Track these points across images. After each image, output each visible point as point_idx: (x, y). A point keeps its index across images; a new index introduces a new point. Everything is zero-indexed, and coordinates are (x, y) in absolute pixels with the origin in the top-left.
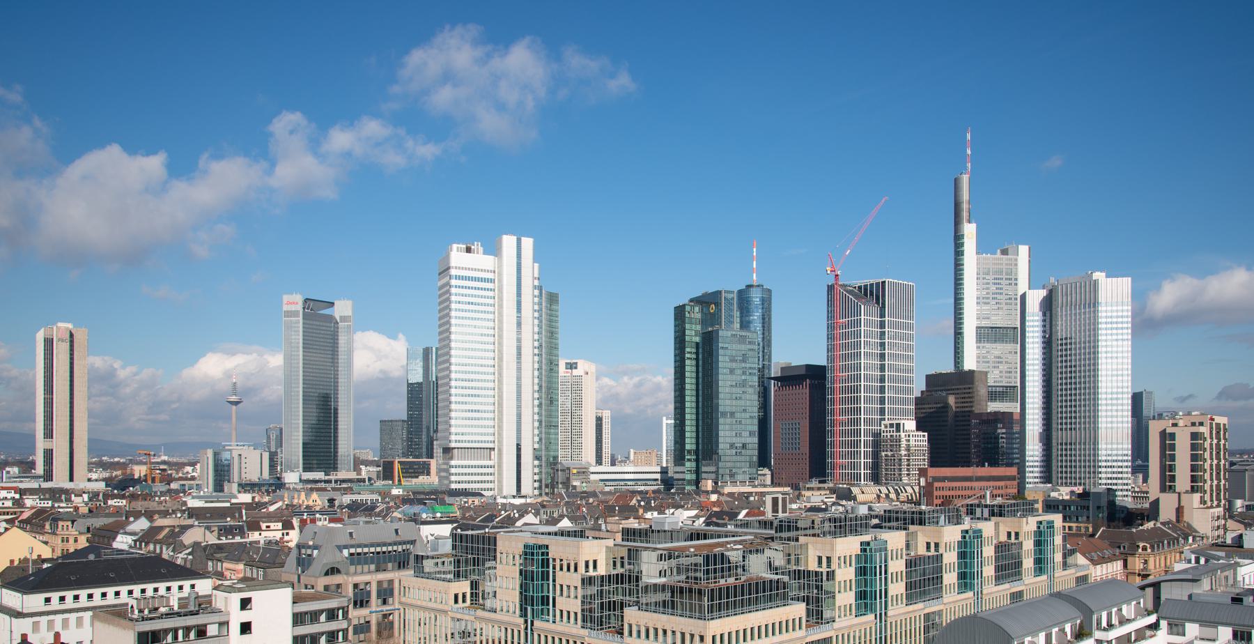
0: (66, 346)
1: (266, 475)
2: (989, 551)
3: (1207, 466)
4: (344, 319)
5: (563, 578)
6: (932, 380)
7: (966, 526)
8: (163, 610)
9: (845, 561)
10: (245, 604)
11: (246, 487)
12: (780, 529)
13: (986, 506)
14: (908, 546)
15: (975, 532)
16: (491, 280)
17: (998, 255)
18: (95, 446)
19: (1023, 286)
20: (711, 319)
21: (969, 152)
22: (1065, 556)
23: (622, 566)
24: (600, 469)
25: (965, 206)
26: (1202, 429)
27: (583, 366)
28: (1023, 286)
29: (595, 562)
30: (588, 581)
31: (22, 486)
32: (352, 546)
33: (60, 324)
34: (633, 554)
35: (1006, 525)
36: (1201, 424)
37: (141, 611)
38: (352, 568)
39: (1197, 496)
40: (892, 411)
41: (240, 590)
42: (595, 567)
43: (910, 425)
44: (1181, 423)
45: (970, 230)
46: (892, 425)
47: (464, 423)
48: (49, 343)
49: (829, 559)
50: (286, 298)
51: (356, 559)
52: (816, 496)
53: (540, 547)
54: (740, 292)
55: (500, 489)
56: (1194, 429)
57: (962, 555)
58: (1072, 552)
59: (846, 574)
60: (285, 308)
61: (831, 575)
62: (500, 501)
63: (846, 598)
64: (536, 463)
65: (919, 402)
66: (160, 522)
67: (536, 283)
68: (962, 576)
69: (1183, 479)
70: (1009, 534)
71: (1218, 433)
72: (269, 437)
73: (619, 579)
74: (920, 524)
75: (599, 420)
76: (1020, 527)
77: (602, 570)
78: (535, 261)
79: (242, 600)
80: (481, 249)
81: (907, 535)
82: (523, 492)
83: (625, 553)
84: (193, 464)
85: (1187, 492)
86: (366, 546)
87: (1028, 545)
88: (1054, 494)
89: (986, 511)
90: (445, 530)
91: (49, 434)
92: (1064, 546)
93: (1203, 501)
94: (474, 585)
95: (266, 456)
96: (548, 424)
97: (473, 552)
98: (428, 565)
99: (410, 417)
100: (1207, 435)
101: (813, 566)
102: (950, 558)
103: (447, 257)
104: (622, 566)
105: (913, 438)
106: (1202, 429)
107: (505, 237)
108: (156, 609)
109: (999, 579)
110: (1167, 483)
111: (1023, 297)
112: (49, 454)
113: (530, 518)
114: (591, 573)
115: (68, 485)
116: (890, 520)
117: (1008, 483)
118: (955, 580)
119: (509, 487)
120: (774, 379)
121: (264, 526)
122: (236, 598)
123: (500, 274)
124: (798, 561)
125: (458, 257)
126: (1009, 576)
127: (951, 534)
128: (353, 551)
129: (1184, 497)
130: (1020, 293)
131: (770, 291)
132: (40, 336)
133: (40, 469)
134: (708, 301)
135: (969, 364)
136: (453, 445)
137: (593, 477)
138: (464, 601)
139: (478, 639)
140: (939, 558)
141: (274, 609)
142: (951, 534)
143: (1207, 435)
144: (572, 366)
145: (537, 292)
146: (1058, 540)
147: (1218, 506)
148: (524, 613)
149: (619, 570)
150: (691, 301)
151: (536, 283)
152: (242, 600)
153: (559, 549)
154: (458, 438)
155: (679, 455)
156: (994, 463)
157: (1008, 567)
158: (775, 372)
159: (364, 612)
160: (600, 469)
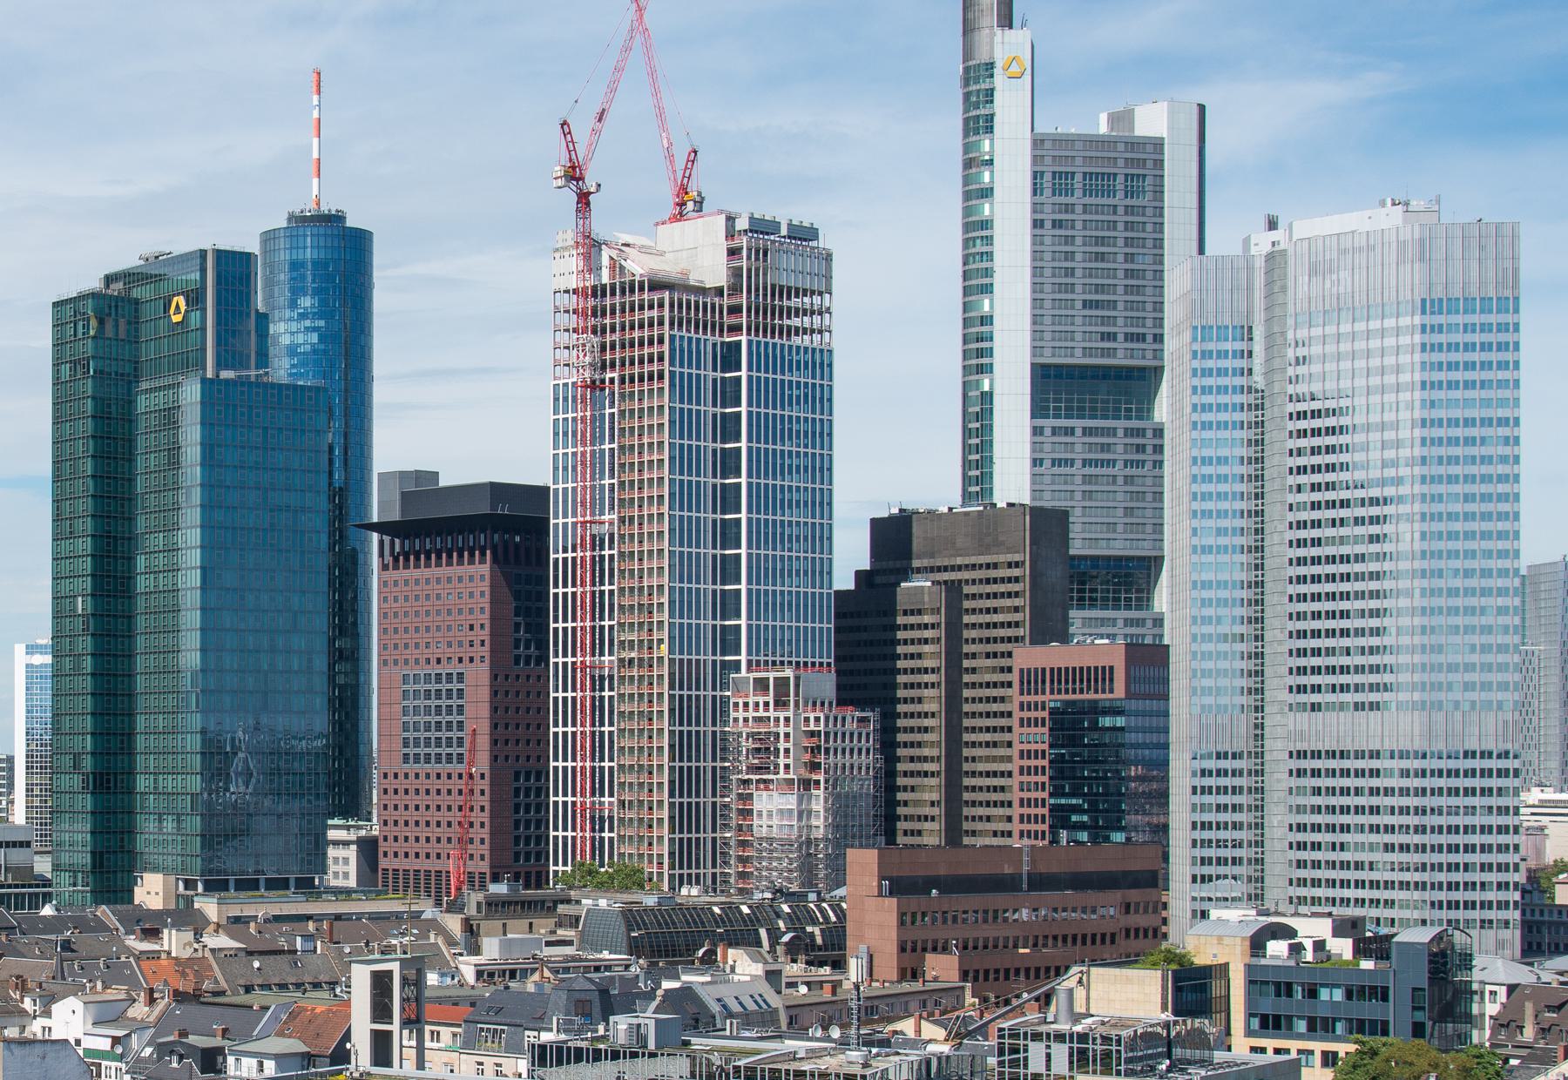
13: (1060, 1037)
120: (380, 528)
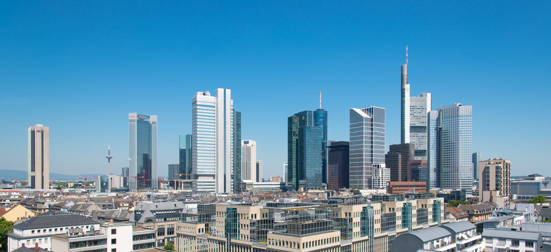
0: (40, 134)
1: (122, 186)
2: (414, 212)
3: (502, 180)
4: (154, 123)
5: (242, 221)
6: (392, 148)
7: (405, 202)
8: (80, 234)
9: (356, 214)
10: (114, 232)
11: (113, 190)
12: (330, 202)
14: (382, 209)
15: (409, 204)
16: (215, 107)
17: (419, 97)
18: (51, 175)
19: (429, 109)
20: (303, 123)
21: (407, 55)
22: (445, 215)
23: (266, 217)
24: (258, 183)
25: (405, 77)
26: (500, 165)
27: (251, 143)
28: (429, 109)
29: (255, 215)
30: (253, 224)
31: (22, 190)
32: (157, 211)
33: (38, 125)
34: (271, 213)
35: (422, 201)
36: (500, 163)
37: (71, 234)
38: (157, 220)
39: (498, 192)
40: (376, 160)
41: (111, 226)
42: (255, 217)
43: (383, 165)
44: (492, 163)
45: (407, 87)
46: (376, 166)
47: (203, 164)
48: (33, 133)
49: (350, 214)
50: (130, 114)
51: (158, 216)
52: (346, 194)
53: (233, 209)
54: (315, 112)
55: (217, 191)
56: (497, 165)
57: (404, 213)
58: (448, 213)
59: (357, 219)
60: (130, 118)
61: (351, 220)
62: (217, 195)
63: (357, 229)
64: (232, 181)
65: (387, 156)
66: (78, 203)
67: (232, 108)
68: (404, 222)
69: (492, 186)
70: (422, 205)
71: (507, 167)
72: (123, 172)
73: (266, 221)
74: (387, 201)
75: (258, 165)
76: (427, 202)
77: (259, 218)
78: (231, 99)
79: (112, 230)
80: (210, 94)
81: (382, 205)
82: (227, 192)
83: (267, 211)
84: (92, 183)
85: (494, 190)
86: (163, 211)
87: (430, 210)
88: (441, 192)
89: (413, 196)
90: (195, 206)
91: (33, 170)
92: (445, 211)
93: (500, 194)
94: (207, 225)
95: (122, 178)
96: (237, 165)
97: (206, 214)
98: (188, 219)
99: (181, 163)
100: (502, 167)
101: (343, 216)
102: (399, 214)
103: (196, 98)
104: (266, 217)
105: (384, 173)
106: (500, 165)
107: (219, 89)
108: (77, 233)
109: (419, 223)
110: (486, 186)
111: (429, 114)
112: (33, 178)
113: (229, 201)
114: (254, 219)
115: (42, 190)
116: (375, 198)
117: (423, 188)
118: (401, 223)
119: (221, 190)
121: (121, 205)
122: (109, 230)
123: (217, 104)
124: (337, 214)
125: (200, 97)
126: (424, 222)
127: (399, 205)
128: (157, 213)
129: (493, 192)
130: (428, 112)
131: (326, 112)
132: (29, 130)
133: (30, 184)
134: (302, 116)
135: (407, 141)
136: (198, 173)
137: (255, 186)
138: (203, 232)
139: (208, 248)
140: (394, 214)
141: (125, 235)
142: (399, 205)
143: (502, 167)
144: (246, 143)
145: (232, 112)
146: (442, 208)
147: (507, 196)
148: (226, 235)
149: (265, 218)
150: (295, 115)
151: (232, 108)
152: (112, 230)
153: (240, 210)
154: (201, 170)
155: (290, 178)
156: (417, 180)
157: (422, 218)
158: (328, 144)
159: (162, 237)
160: (258, 183)
